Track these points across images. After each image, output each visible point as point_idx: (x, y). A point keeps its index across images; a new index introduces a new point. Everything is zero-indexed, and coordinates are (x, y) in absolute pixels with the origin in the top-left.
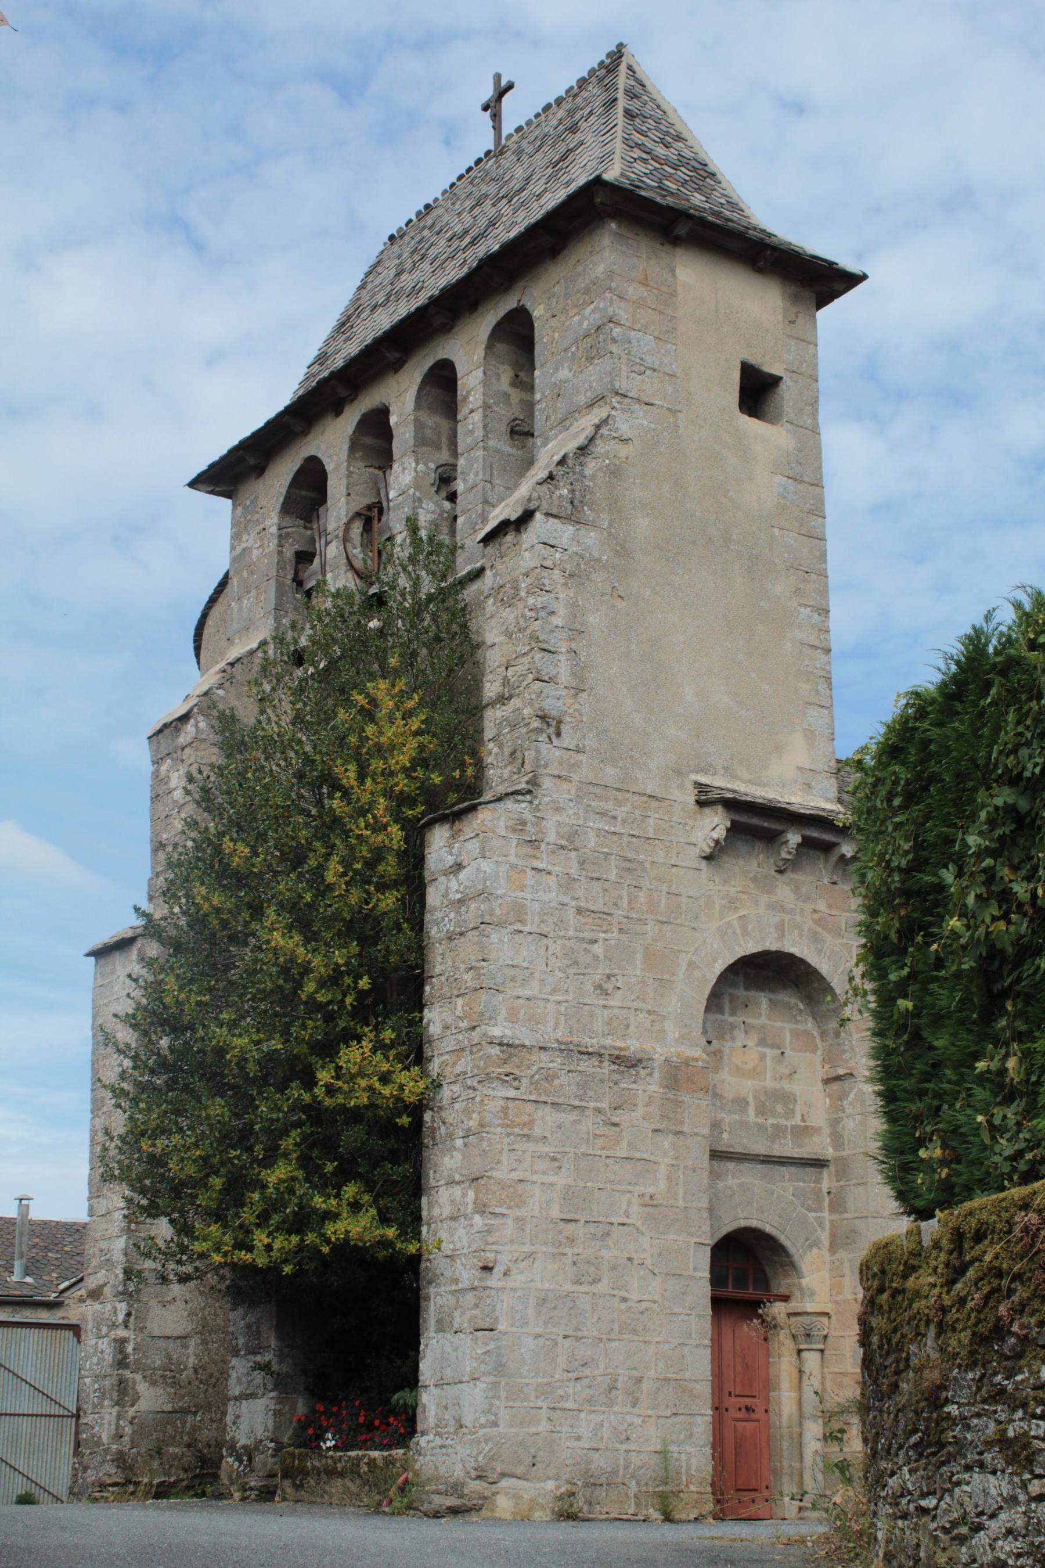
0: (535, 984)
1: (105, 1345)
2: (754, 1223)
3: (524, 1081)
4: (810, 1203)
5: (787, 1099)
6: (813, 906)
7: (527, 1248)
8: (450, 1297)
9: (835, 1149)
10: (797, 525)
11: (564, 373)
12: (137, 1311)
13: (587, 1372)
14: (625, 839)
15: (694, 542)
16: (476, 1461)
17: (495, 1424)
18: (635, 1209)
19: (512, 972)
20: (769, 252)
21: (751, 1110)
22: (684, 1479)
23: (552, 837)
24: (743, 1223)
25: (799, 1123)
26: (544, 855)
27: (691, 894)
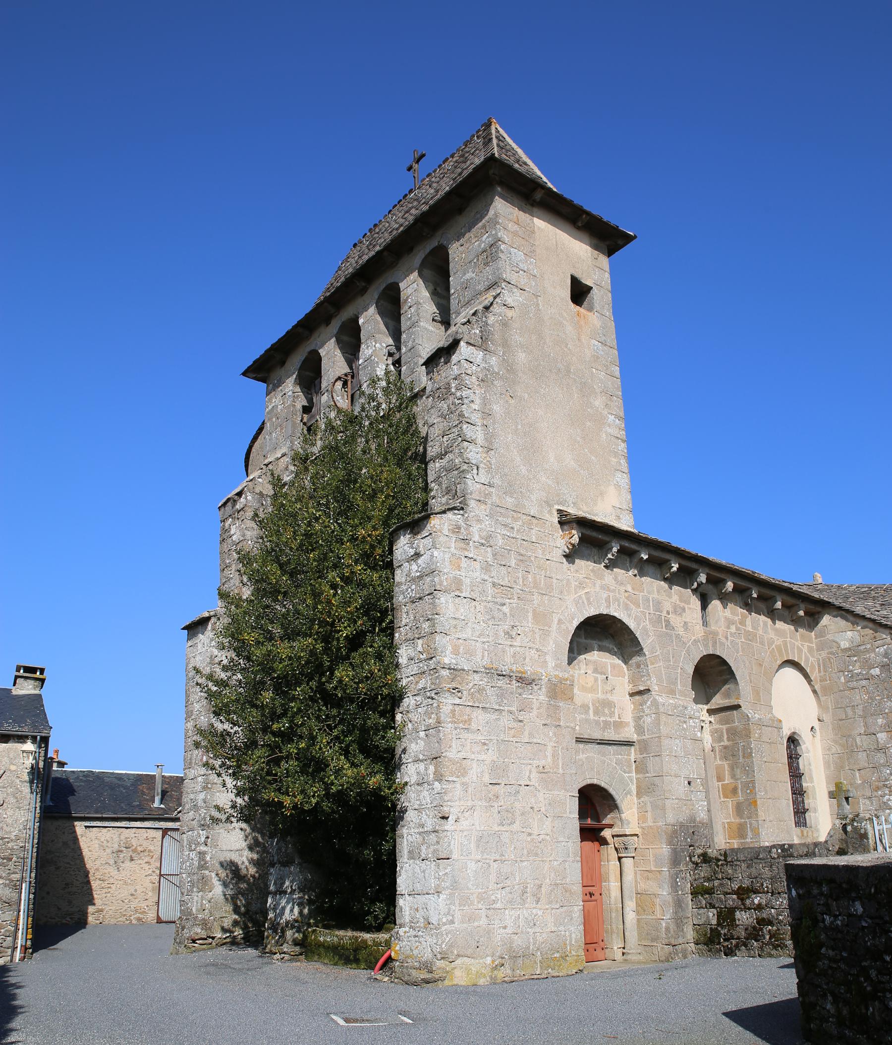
0: (469, 631)
1: (193, 855)
2: (595, 782)
3: (465, 693)
4: (625, 768)
5: (610, 704)
6: (624, 588)
7: (470, 803)
8: (418, 836)
9: (638, 735)
10: (605, 368)
11: (470, 275)
12: (212, 835)
13: (508, 882)
14: (519, 542)
15: (550, 370)
16: (441, 948)
17: (452, 922)
18: (534, 775)
19: (454, 622)
20: (584, 216)
21: (591, 712)
22: (569, 948)
23: (476, 538)
24: (589, 782)
25: (617, 719)
26: (472, 549)
27: (558, 578)
